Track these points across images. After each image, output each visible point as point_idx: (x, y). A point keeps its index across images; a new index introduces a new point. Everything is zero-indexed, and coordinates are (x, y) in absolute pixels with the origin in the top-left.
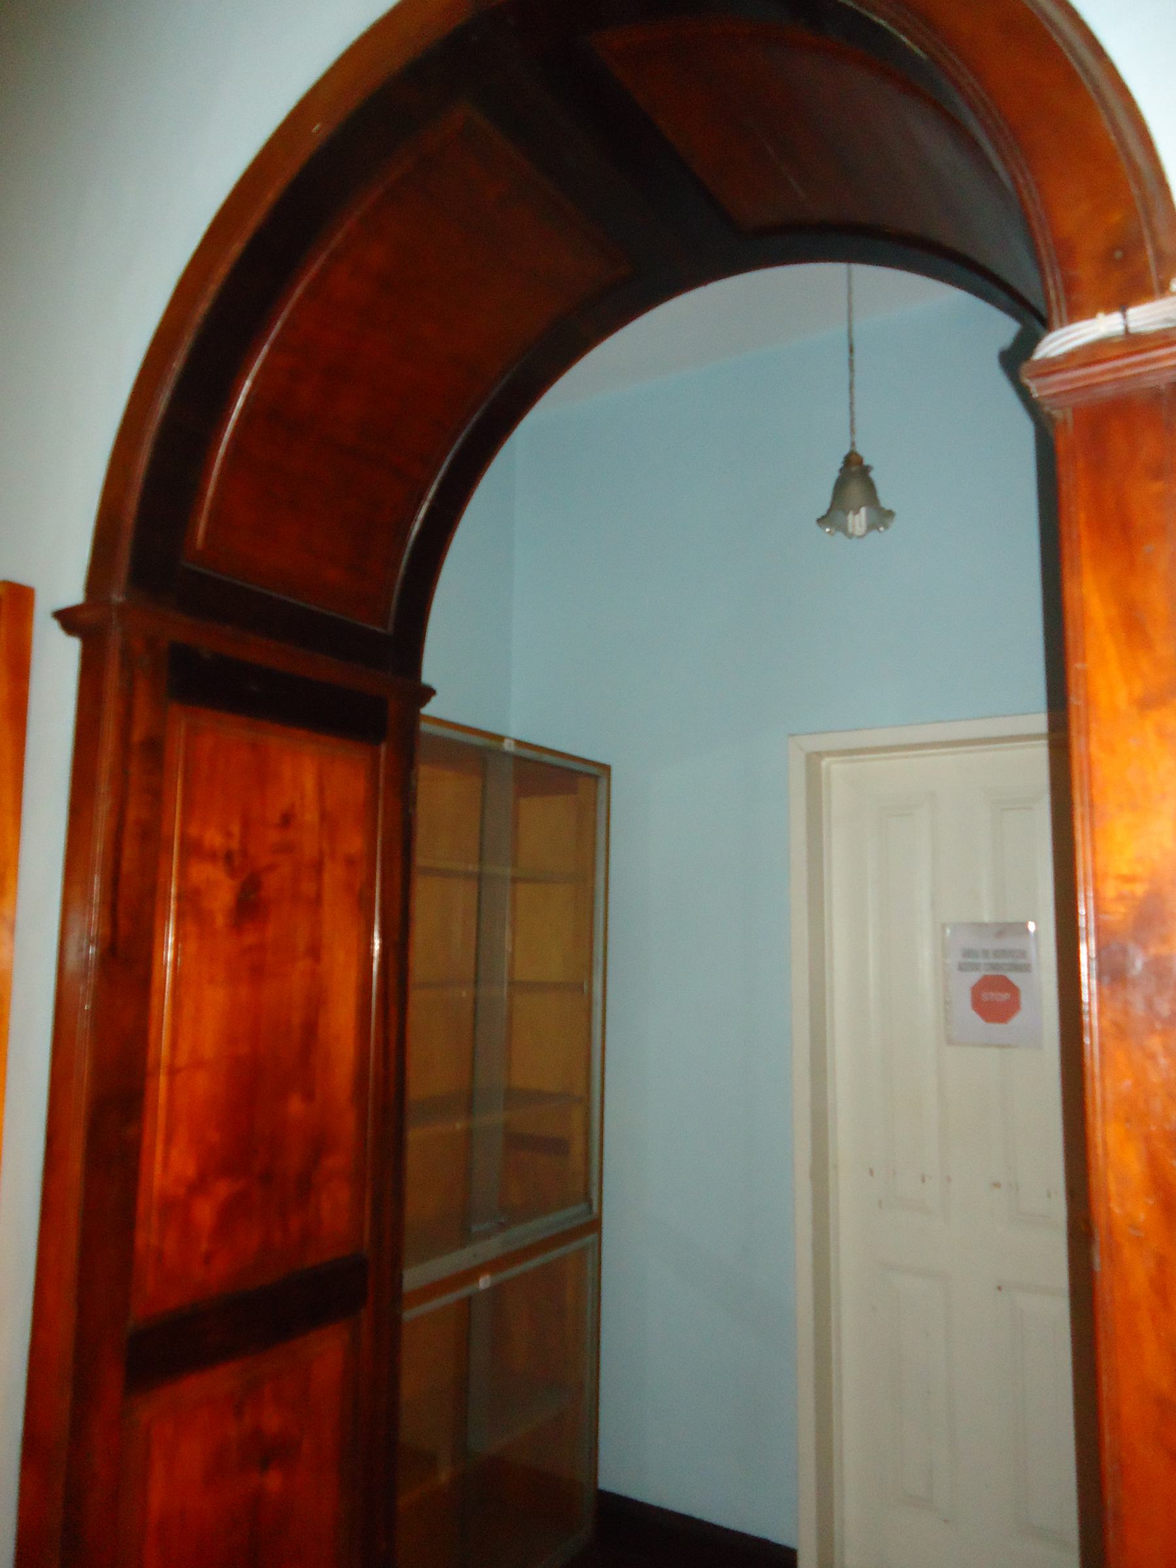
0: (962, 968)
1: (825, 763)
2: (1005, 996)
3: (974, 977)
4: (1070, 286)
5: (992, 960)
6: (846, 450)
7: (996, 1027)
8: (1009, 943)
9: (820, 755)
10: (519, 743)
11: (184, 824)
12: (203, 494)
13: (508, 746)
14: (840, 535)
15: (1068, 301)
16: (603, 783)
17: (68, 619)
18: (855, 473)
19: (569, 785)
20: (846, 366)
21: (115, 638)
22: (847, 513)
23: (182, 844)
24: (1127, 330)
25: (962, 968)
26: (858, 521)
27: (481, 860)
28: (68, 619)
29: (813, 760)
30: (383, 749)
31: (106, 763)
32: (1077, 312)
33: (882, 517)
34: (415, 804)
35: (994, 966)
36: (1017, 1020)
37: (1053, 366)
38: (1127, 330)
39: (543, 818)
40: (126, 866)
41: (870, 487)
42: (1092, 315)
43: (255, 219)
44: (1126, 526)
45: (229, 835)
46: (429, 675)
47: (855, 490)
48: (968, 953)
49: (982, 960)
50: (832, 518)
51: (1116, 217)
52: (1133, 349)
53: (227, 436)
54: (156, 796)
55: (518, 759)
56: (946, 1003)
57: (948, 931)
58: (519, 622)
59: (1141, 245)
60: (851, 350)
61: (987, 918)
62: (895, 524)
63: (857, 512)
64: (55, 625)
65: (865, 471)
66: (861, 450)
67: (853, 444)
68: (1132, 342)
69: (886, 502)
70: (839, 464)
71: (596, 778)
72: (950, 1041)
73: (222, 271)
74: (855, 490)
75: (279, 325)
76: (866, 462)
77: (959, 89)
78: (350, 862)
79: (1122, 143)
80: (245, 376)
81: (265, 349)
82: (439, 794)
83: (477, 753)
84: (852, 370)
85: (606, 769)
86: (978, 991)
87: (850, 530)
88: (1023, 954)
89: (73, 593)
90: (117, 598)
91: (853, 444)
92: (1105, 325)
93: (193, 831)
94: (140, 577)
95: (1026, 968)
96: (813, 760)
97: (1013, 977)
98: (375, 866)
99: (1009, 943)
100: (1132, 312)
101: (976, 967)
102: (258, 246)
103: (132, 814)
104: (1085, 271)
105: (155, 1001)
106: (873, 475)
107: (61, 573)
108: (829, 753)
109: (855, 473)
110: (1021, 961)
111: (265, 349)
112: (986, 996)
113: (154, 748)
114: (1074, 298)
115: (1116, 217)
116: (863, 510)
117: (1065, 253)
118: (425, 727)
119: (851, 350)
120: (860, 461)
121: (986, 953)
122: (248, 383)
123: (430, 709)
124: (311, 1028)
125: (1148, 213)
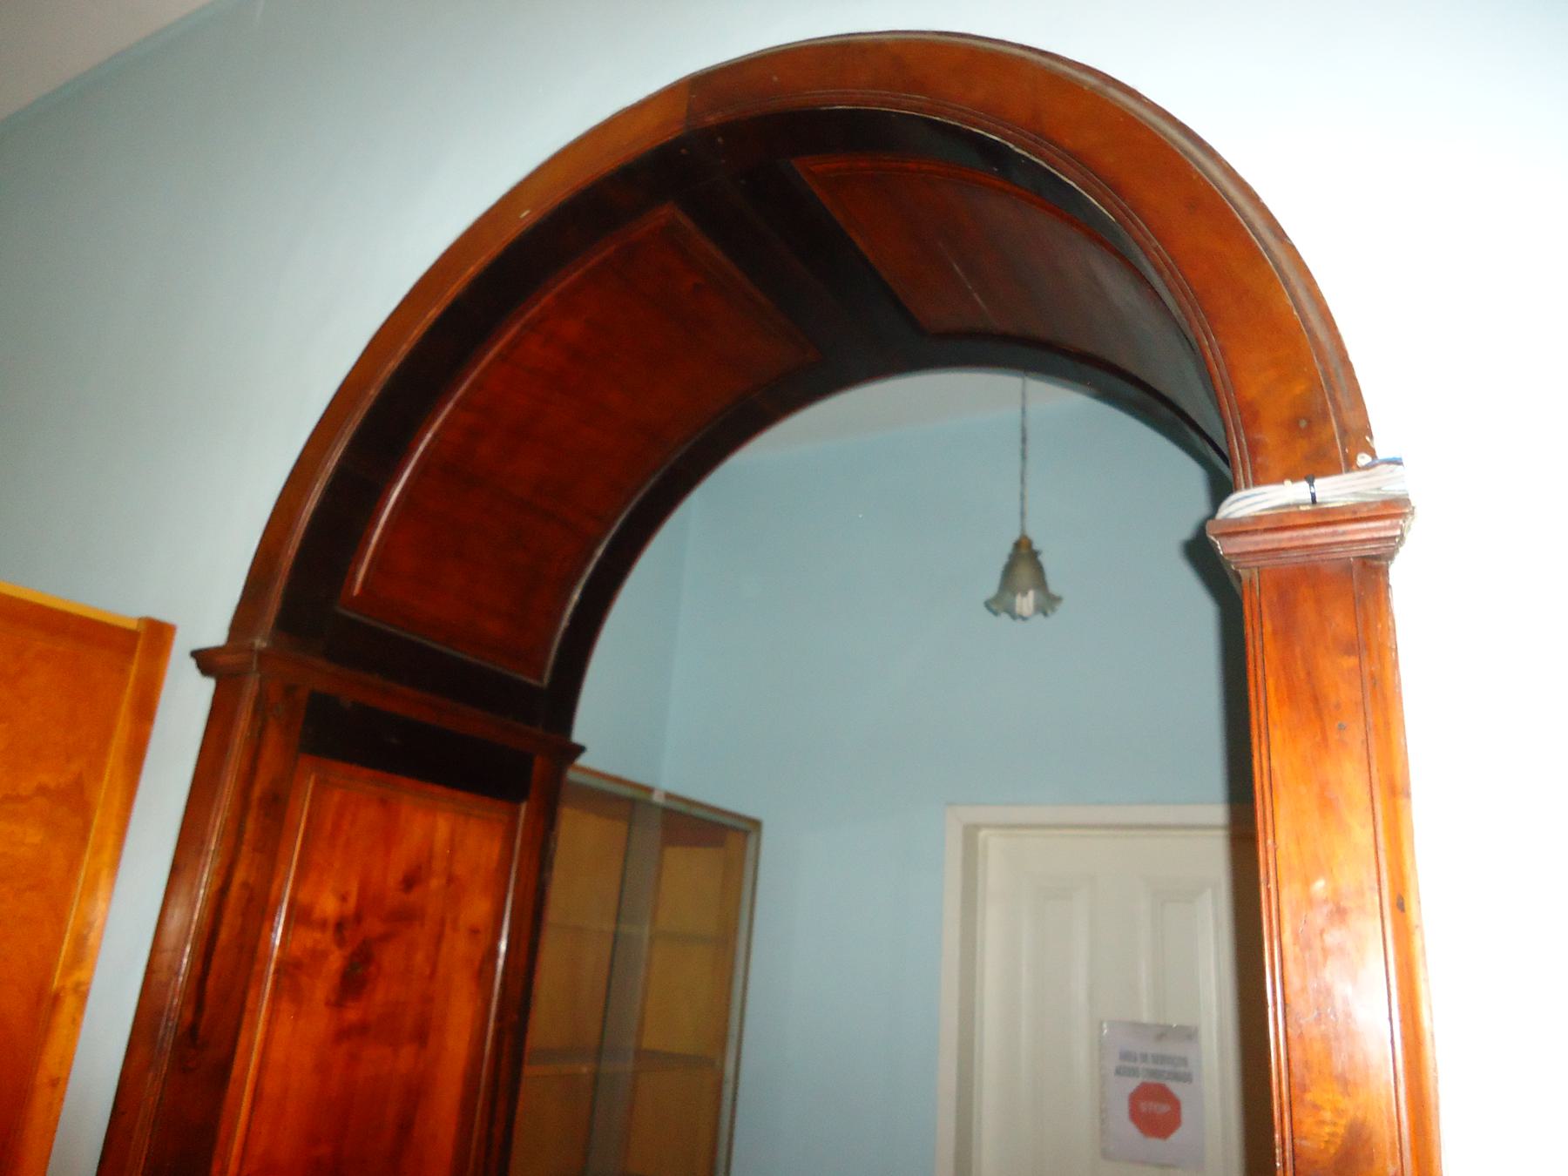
0: (1118, 1072)
1: (983, 833)
2: (1164, 1108)
3: (1132, 1084)
4: (1254, 448)
5: (1152, 1066)
6: (1016, 536)
7: (1155, 1143)
9: (978, 827)
10: (669, 796)
11: (295, 889)
12: (368, 543)
13: (657, 798)
14: (1005, 617)
15: (1253, 462)
16: (752, 840)
17: (205, 660)
18: (1024, 560)
19: (721, 837)
20: (1018, 457)
21: (251, 687)
22: (1015, 595)
23: (291, 905)
24: (1311, 484)
26: (1026, 603)
27: (617, 919)
28: (205, 660)
29: (970, 833)
30: (523, 808)
31: (219, 820)
32: (1260, 478)
33: (1048, 603)
34: (551, 867)
35: (1153, 1073)
37: (1239, 529)
38: (1311, 484)
39: (687, 868)
40: (224, 934)
41: (1039, 570)
42: (1280, 481)
43: (454, 289)
44: (1316, 699)
45: (344, 898)
46: (578, 735)
47: (1024, 573)
48: (1125, 1056)
49: (1141, 1066)
50: (1000, 604)
51: (1299, 388)
52: (1319, 520)
53: (421, 448)
54: (270, 850)
55: (667, 811)
56: (1102, 1111)
58: (679, 670)
59: (1325, 416)
60: (1024, 440)
61: (1146, 1017)
62: (1062, 609)
63: (1025, 593)
64: (192, 663)
65: (1033, 556)
68: (1322, 516)
69: (1054, 587)
70: (1008, 548)
71: (746, 833)
72: (1105, 1155)
73: (416, 333)
74: (1024, 573)
76: (1036, 546)
77: (1146, 253)
78: (474, 931)
79: (1305, 320)
81: (450, 406)
82: (578, 833)
83: (625, 804)
84: (1024, 457)
85: (756, 824)
86: (1136, 1098)
87: (1018, 610)
88: (1184, 1061)
89: (215, 634)
90: (260, 643)
92: (1292, 493)
93: (304, 897)
94: (287, 623)
95: (1186, 1078)
96: (970, 833)
97: (1175, 1088)
98: (509, 873)
99: (1173, 1049)
100: (1319, 483)
101: (1133, 1072)
102: (454, 312)
103: (240, 876)
104: (1269, 437)
105: (232, 1089)
106: (1043, 559)
107: (207, 617)
108: (988, 826)
109: (1024, 560)
110: (1181, 1069)
111: (450, 406)
112: (1144, 1106)
113: (276, 806)
114: (1259, 459)
115: (1299, 388)
116: (1031, 594)
117: (1251, 416)
118: (572, 775)
119: (1024, 440)
120: (1029, 544)
121: (1144, 1057)
122: (429, 436)
123: (583, 761)
124: (405, 1127)
125: (1331, 388)
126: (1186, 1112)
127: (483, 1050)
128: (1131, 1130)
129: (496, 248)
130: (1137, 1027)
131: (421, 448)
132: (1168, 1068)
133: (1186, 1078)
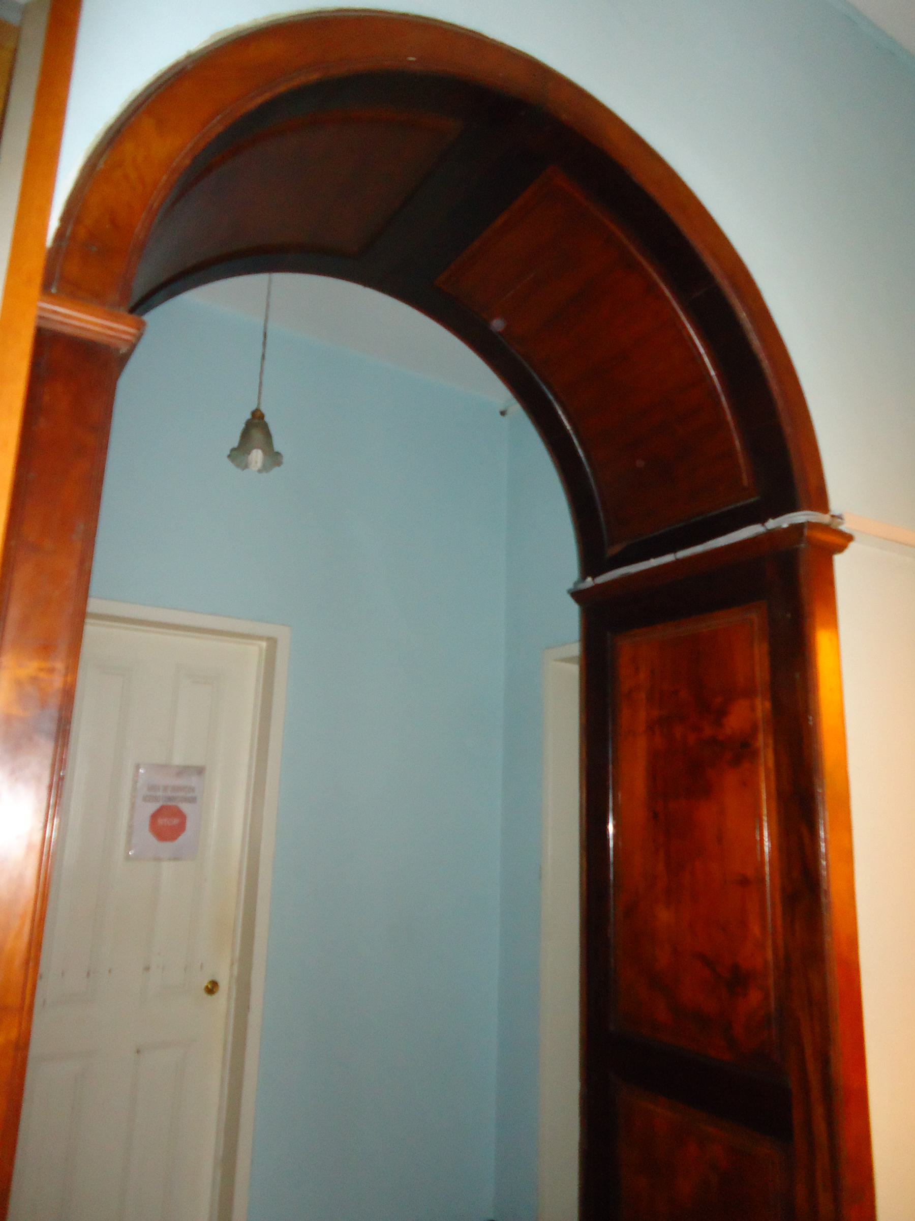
2: (176, 821)
3: (153, 807)
8: (193, 781)
18: (256, 427)
25: (146, 799)
26: (257, 456)
33: (274, 458)
35: (170, 799)
36: (182, 839)
41: (268, 435)
47: (257, 435)
48: (152, 788)
49: (160, 793)
50: (239, 454)
53: (698, 342)
57: (141, 771)
66: (264, 409)
67: (259, 404)
69: (278, 445)
70: (248, 416)
75: (729, 417)
80: (718, 375)
91: (259, 404)
97: (185, 807)
101: (155, 799)
106: (267, 419)
109: (256, 427)
110: (190, 795)
121: (165, 788)
126: (189, 824)
127: (613, 748)
128: (152, 839)
129: (666, 203)
130: (163, 767)
131: (698, 342)
132: (181, 794)
133: (193, 800)
